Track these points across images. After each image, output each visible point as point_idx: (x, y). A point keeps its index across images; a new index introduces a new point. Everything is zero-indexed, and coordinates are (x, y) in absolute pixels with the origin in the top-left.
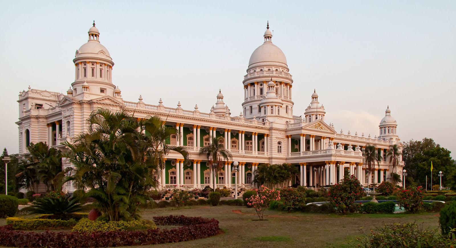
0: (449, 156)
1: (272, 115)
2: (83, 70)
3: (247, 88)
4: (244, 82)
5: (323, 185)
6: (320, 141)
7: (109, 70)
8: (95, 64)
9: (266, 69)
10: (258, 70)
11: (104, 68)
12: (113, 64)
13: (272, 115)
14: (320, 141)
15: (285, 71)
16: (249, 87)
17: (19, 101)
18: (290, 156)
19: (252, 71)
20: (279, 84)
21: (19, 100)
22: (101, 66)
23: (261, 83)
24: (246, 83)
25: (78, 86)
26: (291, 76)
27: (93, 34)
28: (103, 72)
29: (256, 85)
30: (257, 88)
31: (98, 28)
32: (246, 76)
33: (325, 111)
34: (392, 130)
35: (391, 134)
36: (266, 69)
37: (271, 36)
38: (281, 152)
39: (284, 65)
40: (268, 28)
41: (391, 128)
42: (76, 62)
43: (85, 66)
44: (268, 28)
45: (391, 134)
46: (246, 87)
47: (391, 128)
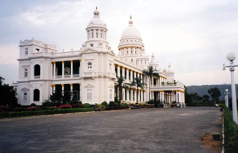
0: (220, 92)
1: (145, 65)
2: (92, 34)
3: (120, 50)
4: (118, 47)
5: (166, 102)
6: (159, 80)
7: (103, 33)
8: (98, 31)
9: (134, 40)
10: (126, 41)
11: (103, 33)
12: (107, 30)
13: (145, 65)
14: (159, 80)
15: (140, 41)
16: (121, 49)
17: (19, 60)
18: (161, 87)
19: (122, 41)
20: (137, 48)
21: (19, 59)
22: (97, 31)
23: (132, 48)
24: (120, 47)
25: (94, 43)
26: (143, 43)
27: (96, 14)
28: (102, 34)
29: (125, 49)
30: (129, 50)
31: (99, 10)
32: (120, 44)
33: (158, 64)
34: (101, 34)
35: (172, 77)
36: (134, 40)
37: (106, 31)
38: (27, 76)
39: (139, 38)
40: (131, 18)
41: (134, 48)
42: (87, 30)
43: (93, 32)
44: (131, 18)
45: (172, 77)
46: (120, 49)
47: (134, 48)
